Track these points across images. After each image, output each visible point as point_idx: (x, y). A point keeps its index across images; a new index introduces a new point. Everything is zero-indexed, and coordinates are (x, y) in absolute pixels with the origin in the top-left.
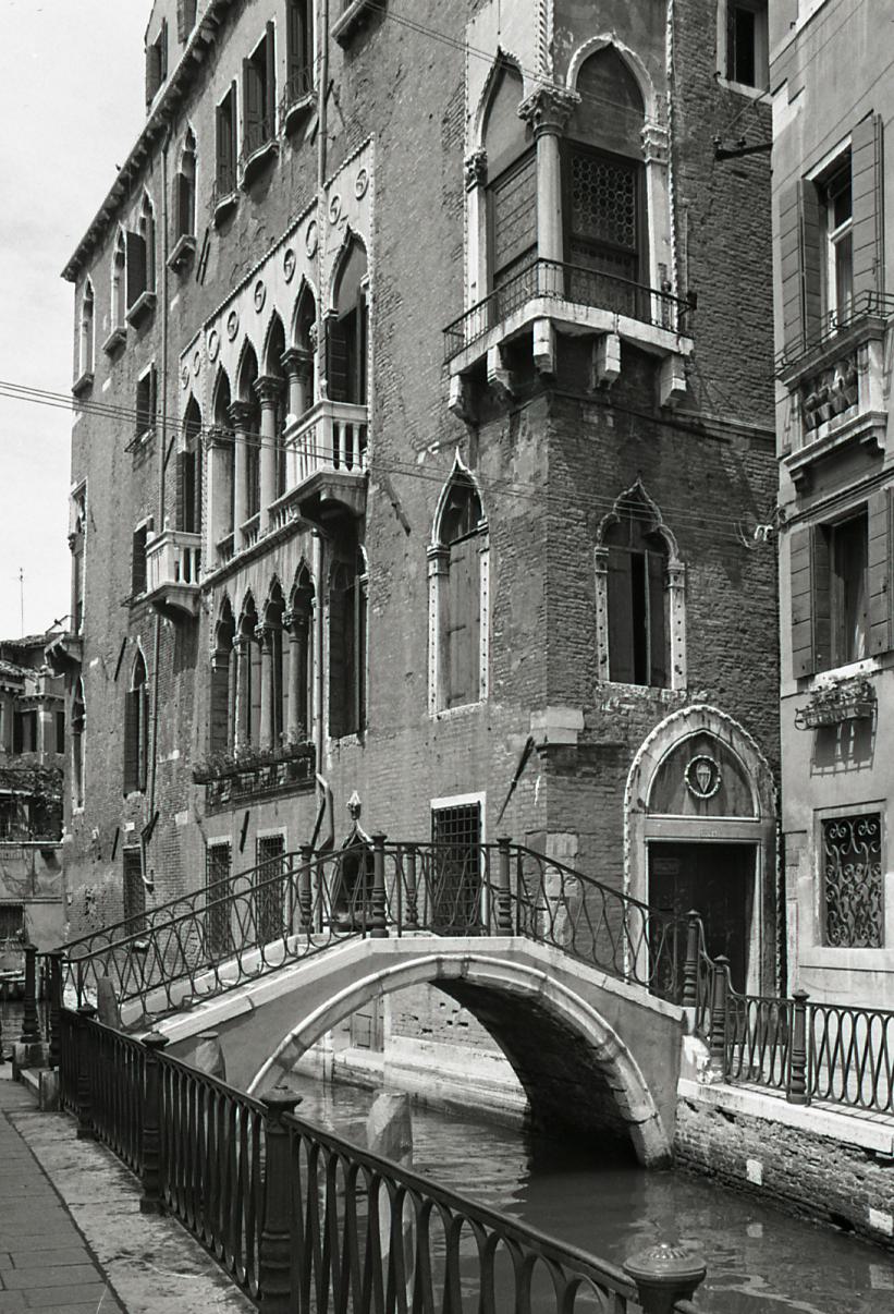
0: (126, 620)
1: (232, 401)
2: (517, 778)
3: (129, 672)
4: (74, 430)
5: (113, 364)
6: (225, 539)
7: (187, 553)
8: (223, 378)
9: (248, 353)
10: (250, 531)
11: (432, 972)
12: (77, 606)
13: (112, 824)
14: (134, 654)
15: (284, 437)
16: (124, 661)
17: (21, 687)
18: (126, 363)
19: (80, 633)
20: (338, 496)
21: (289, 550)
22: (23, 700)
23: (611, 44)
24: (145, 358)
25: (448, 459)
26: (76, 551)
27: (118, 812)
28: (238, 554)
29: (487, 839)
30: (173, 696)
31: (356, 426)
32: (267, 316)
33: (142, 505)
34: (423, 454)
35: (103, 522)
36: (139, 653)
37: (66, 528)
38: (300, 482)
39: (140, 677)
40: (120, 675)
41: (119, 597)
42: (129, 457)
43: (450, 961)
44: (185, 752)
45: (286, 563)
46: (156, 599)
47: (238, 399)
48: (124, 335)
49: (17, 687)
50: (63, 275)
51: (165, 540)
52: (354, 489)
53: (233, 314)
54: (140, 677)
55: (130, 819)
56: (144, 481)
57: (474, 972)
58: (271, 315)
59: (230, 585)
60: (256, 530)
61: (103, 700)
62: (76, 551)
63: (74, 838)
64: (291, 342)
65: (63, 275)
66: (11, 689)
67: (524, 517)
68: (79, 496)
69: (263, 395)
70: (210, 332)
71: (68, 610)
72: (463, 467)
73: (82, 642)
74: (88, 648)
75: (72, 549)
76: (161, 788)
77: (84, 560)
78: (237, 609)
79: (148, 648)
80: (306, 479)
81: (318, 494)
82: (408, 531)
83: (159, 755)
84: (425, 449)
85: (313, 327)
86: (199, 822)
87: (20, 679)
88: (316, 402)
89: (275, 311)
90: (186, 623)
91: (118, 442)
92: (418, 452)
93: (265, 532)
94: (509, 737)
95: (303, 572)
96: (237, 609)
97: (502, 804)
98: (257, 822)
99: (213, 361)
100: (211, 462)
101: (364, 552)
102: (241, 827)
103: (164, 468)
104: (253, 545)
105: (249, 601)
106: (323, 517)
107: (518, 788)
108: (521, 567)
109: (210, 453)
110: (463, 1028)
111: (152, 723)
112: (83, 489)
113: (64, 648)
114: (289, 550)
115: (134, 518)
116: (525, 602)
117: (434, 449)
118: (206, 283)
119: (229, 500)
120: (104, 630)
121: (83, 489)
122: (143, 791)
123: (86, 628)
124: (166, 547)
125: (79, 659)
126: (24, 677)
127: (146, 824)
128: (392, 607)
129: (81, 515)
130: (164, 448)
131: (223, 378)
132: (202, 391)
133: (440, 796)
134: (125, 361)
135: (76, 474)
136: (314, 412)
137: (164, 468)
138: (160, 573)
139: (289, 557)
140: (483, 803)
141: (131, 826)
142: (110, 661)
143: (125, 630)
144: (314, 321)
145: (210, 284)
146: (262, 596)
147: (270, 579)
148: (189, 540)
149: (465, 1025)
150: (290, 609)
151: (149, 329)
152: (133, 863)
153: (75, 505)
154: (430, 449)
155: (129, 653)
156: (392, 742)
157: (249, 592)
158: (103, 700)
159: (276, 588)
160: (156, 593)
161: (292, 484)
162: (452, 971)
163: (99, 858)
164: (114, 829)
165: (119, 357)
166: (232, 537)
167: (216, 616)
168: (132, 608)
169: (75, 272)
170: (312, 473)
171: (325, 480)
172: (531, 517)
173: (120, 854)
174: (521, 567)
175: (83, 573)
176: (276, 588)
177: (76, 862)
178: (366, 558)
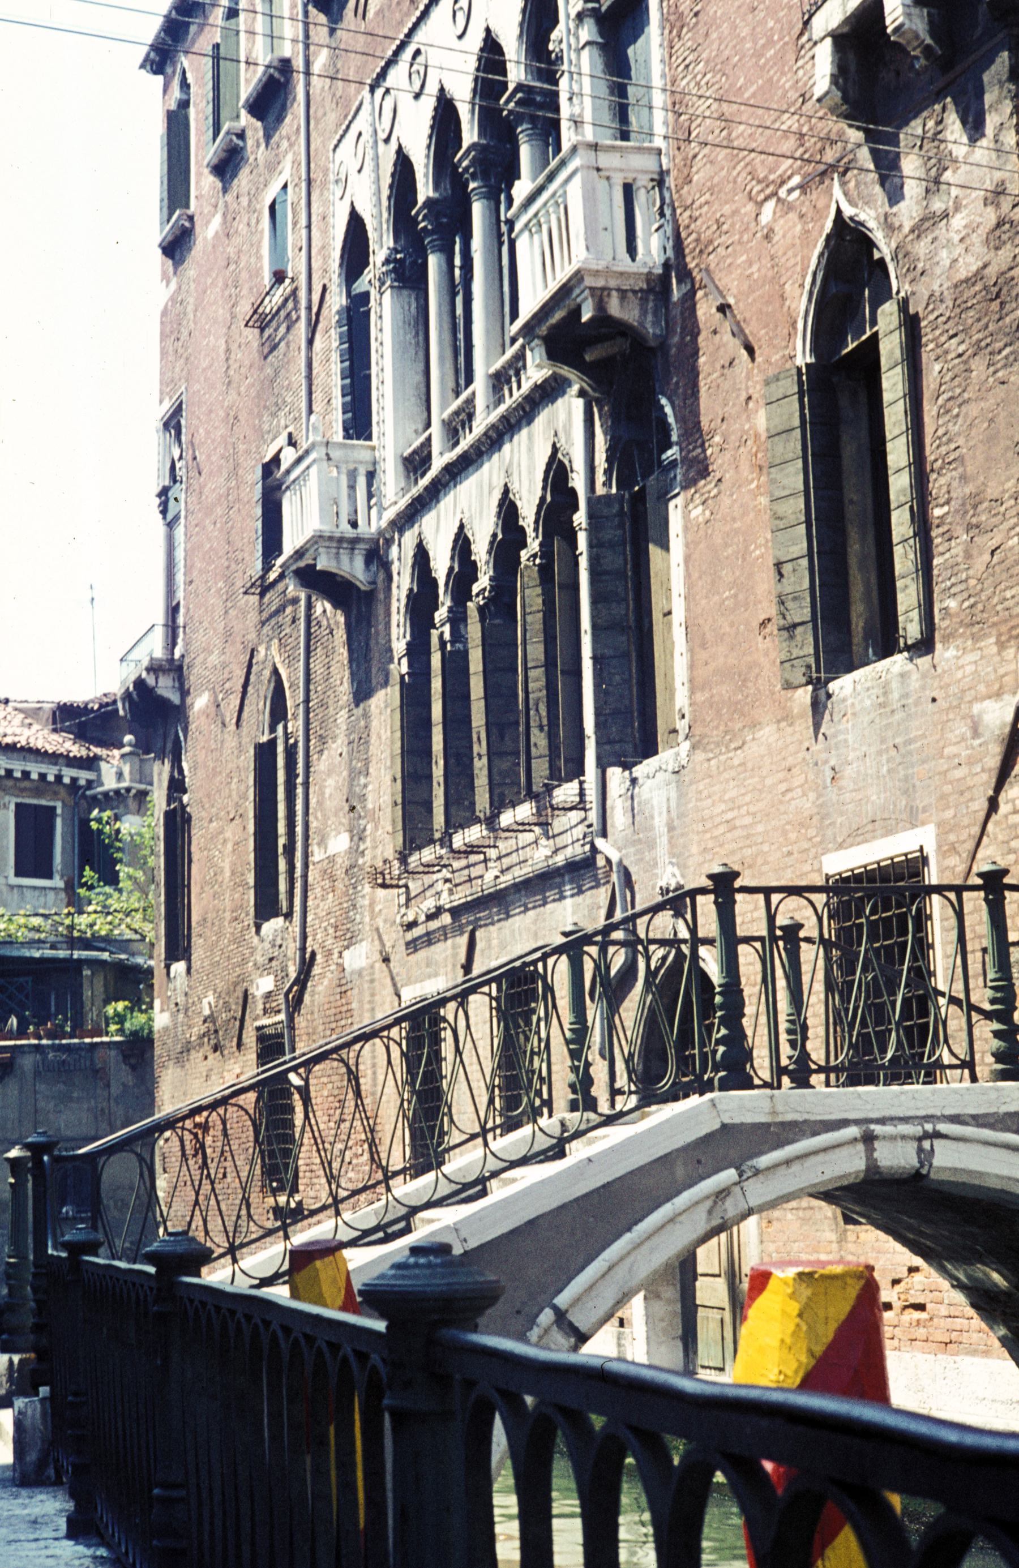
0: (253, 617)
1: (421, 199)
2: (999, 787)
3: (258, 706)
4: (164, 313)
5: (225, 190)
6: (416, 444)
7: (352, 475)
8: (403, 164)
9: (445, 113)
10: (458, 424)
11: (850, 1164)
12: (173, 611)
13: (236, 984)
14: (267, 673)
15: (511, 223)
16: (250, 689)
17: (91, 775)
18: (244, 182)
19: (177, 655)
20: (615, 308)
21: (530, 437)
22: (94, 797)
23: (872, 1167)
24: (273, 167)
25: (820, 204)
26: (170, 516)
27: (244, 961)
28: (438, 463)
29: (942, 871)
30: (334, 738)
31: (643, 181)
32: (475, 41)
33: (274, 415)
34: (771, 204)
35: (209, 455)
36: (275, 672)
37: (154, 481)
38: (543, 295)
39: (278, 712)
40: (245, 715)
41: (240, 582)
42: (252, 335)
43: (893, 1138)
44: (358, 836)
45: (521, 468)
46: (302, 564)
47: (431, 193)
48: (241, 135)
49: (84, 776)
50: (142, 66)
51: (313, 456)
52: (643, 295)
53: (418, 52)
54: (278, 712)
55: (265, 969)
56: (277, 373)
57: (949, 1159)
58: (483, 35)
59: (428, 522)
60: (471, 416)
61: (218, 765)
62: (170, 516)
63: (174, 1016)
64: (516, 73)
65: (142, 66)
66: (74, 780)
67: (978, 275)
68: (173, 424)
69: (474, 177)
70: (379, 92)
71: (159, 616)
72: (848, 211)
73: (180, 668)
74: (193, 679)
75: (164, 512)
76: (322, 905)
77: (180, 532)
78: (441, 564)
79: (290, 660)
80: (553, 286)
81: (577, 312)
82: (750, 350)
83: (314, 848)
84: (775, 194)
85: (554, 35)
86: (386, 960)
87: (90, 763)
88: (566, 146)
89: (488, 30)
90: (359, 604)
91: (233, 316)
92: (761, 204)
93: (483, 421)
94: (976, 708)
95: (557, 472)
96: (441, 564)
97: (970, 845)
98: (489, 947)
99: (387, 141)
100: (386, 313)
101: (668, 410)
102: (462, 958)
103: (310, 342)
104: (465, 443)
105: (462, 544)
106: (588, 358)
107: (1004, 808)
108: (978, 365)
109: (387, 296)
110: (917, 1315)
111: (300, 790)
112: (178, 411)
113: (151, 681)
114: (530, 437)
115: (263, 437)
116: (991, 439)
117: (790, 191)
118: (371, 14)
119: (420, 378)
120: (217, 641)
121: (178, 411)
122: (289, 915)
123: (187, 644)
124: (314, 470)
125: (175, 698)
126: (97, 758)
127: (293, 975)
128: (726, 501)
129: (176, 453)
130: (309, 308)
131: (403, 164)
132: (368, 196)
133: (841, 846)
134: (243, 180)
135: (167, 383)
136: (563, 163)
137: (310, 342)
138: (302, 522)
139: (530, 450)
140: (930, 851)
141: (265, 984)
142: (228, 693)
143: (252, 636)
144: (556, 22)
145: (377, 14)
146: (483, 533)
147: (497, 495)
148: (359, 451)
149: (920, 1307)
150: (534, 545)
151: (280, 119)
152: (270, 1046)
153: (169, 438)
154: (782, 193)
155: (260, 673)
156: (738, 757)
157: (462, 527)
158: (218, 765)
159: (508, 510)
160: (299, 554)
161: (529, 305)
162: (896, 1156)
163: (216, 1048)
164: (239, 993)
165: (234, 175)
166: (429, 439)
167: (403, 582)
168: (262, 595)
169: (161, 58)
170: (562, 274)
171: (589, 281)
172: (992, 272)
173: (250, 1038)
174: (978, 365)
175: (180, 554)
176: (508, 510)
177: (178, 1061)
178: (671, 419)
